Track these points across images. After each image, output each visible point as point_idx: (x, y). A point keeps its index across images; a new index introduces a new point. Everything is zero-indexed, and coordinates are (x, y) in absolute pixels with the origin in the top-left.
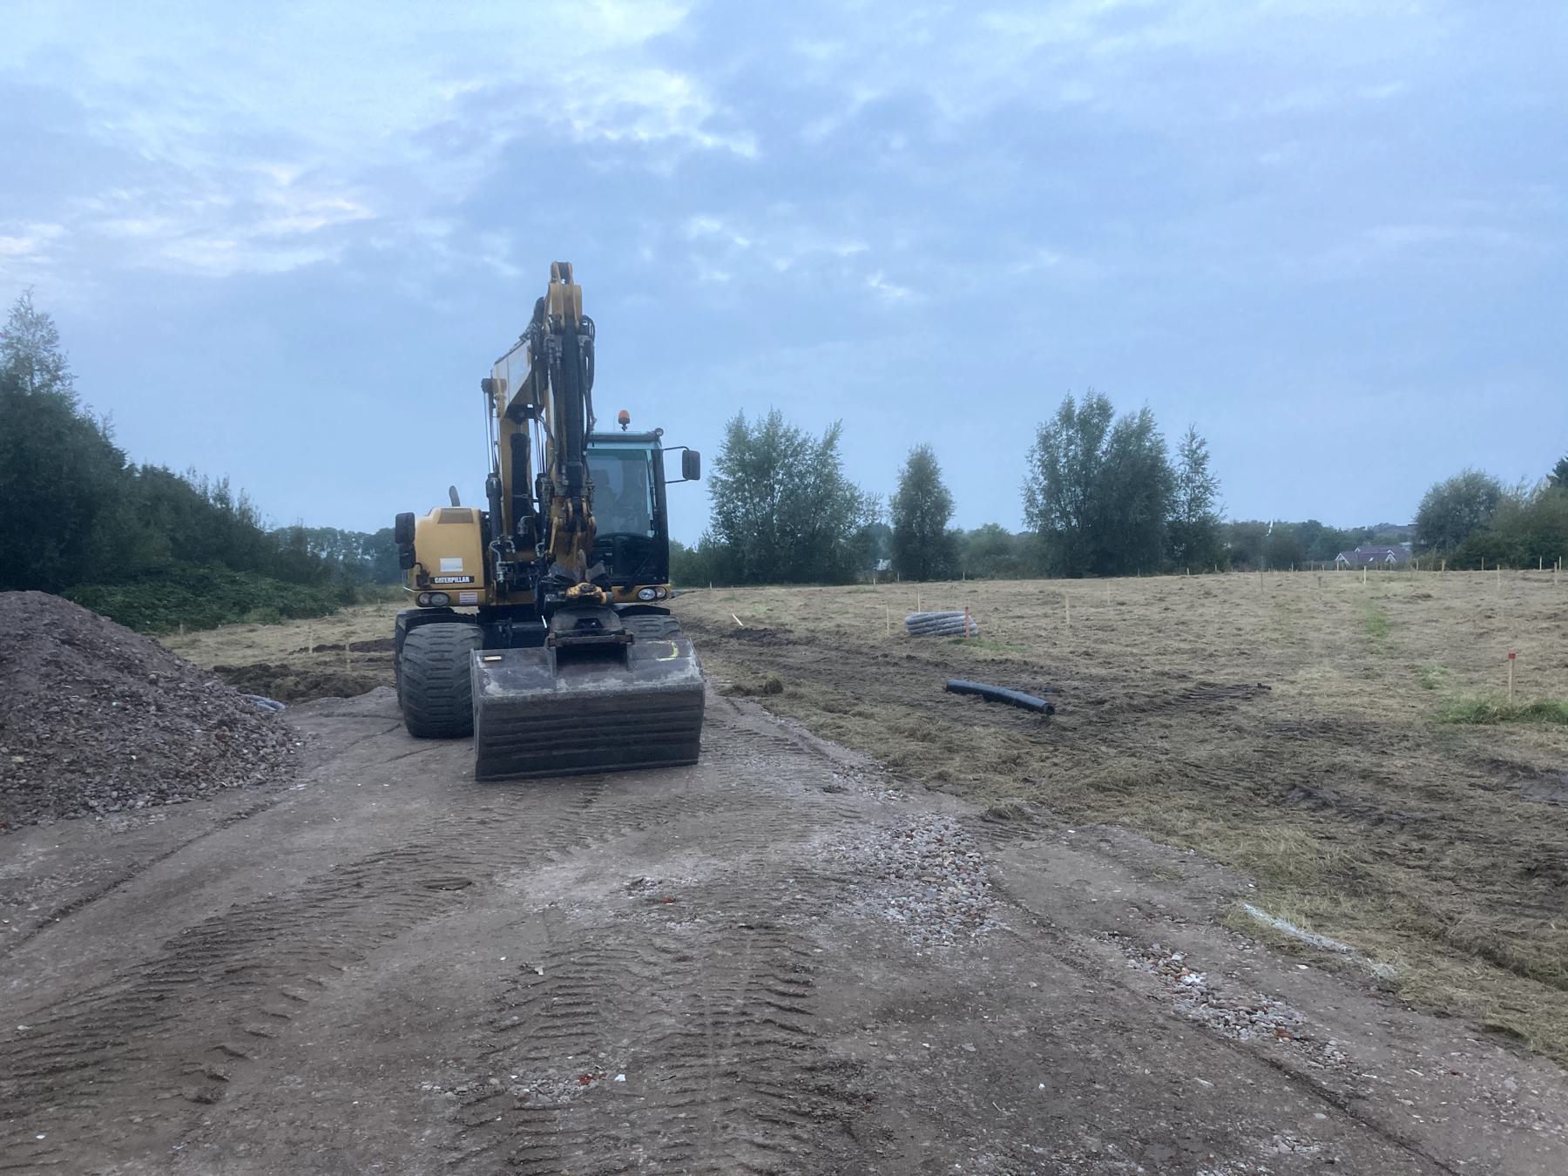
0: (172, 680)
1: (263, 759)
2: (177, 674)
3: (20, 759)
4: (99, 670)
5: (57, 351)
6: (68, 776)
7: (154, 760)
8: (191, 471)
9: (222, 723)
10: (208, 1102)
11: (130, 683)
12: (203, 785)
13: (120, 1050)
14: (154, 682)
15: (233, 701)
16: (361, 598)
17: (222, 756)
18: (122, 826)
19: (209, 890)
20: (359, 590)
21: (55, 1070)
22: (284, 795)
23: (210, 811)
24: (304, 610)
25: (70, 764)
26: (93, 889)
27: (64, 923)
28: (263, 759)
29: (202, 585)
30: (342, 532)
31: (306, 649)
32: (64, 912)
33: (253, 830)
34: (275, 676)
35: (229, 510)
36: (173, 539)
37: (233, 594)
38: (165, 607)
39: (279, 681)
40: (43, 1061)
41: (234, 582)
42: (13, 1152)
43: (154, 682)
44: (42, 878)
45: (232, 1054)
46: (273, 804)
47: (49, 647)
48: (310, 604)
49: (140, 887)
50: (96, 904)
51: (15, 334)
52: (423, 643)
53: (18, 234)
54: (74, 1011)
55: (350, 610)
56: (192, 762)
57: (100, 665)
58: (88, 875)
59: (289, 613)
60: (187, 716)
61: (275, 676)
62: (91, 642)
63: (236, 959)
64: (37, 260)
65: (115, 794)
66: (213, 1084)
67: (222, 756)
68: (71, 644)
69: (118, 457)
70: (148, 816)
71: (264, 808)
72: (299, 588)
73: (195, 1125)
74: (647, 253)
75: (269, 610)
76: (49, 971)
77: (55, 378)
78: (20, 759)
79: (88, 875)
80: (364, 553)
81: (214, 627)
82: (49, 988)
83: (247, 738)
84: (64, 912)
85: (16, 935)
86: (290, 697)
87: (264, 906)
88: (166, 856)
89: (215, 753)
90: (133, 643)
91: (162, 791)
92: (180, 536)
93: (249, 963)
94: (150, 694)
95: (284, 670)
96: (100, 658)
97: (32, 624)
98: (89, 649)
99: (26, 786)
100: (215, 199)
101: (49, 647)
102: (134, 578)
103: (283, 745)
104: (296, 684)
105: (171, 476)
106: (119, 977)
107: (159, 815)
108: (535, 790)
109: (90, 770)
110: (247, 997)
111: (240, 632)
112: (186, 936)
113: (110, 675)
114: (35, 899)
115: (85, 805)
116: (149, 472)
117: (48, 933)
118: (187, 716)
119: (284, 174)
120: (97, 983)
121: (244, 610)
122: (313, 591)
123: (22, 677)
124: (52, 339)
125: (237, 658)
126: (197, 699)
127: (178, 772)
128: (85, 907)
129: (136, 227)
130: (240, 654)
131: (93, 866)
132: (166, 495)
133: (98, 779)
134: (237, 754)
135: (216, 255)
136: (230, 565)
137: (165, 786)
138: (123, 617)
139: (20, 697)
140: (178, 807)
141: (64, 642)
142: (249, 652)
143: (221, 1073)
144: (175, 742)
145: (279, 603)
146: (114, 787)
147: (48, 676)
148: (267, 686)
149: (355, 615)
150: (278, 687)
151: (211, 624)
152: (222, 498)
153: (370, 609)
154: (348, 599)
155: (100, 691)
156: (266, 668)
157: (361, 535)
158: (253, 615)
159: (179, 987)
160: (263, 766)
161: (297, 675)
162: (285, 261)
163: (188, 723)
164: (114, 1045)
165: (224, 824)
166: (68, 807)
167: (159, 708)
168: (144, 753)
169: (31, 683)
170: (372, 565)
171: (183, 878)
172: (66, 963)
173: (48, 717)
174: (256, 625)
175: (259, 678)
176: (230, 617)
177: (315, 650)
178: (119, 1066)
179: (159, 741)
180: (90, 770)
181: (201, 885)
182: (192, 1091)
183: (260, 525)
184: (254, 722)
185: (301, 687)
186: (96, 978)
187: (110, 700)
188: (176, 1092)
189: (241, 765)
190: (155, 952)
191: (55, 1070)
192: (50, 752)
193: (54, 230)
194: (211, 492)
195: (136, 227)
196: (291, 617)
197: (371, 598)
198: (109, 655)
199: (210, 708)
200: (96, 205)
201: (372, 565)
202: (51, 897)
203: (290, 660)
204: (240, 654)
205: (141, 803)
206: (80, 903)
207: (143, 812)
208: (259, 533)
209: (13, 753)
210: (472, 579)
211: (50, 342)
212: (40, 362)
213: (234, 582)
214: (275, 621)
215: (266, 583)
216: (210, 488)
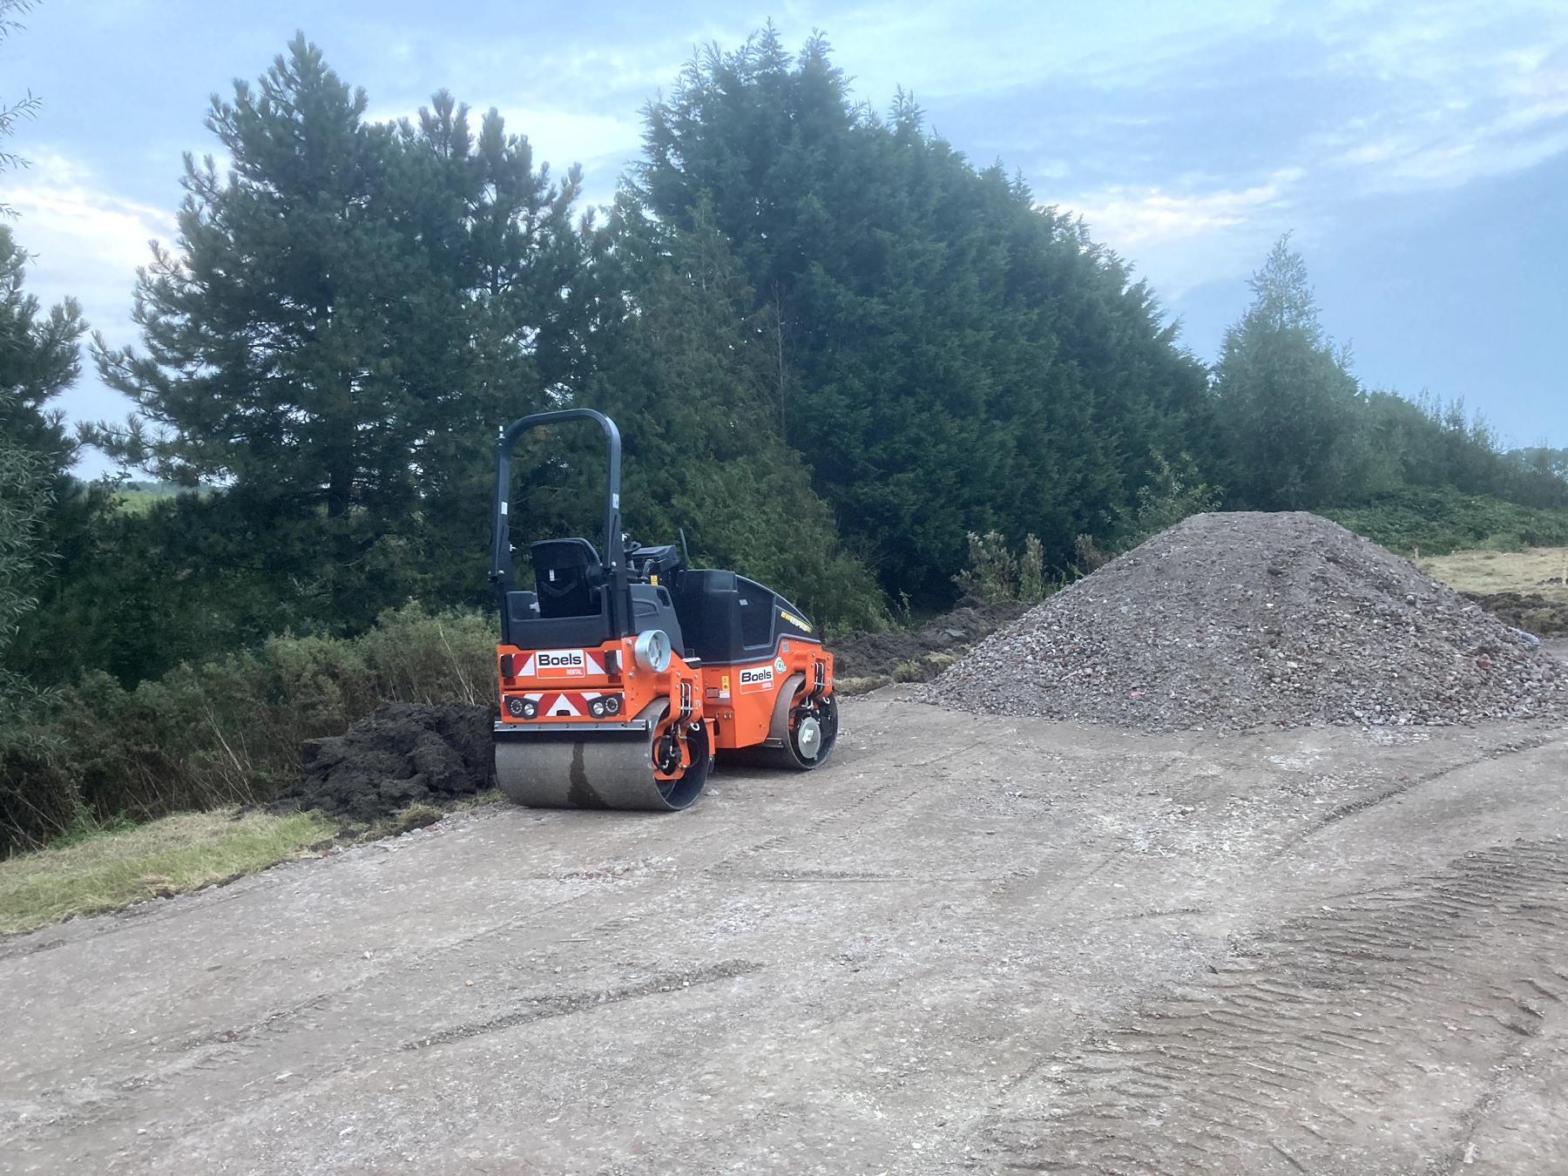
0: (1429, 602)
1: (1528, 692)
2: (1434, 597)
3: (1294, 665)
4: (1360, 588)
5: (1304, 288)
6: (1337, 685)
7: (1415, 680)
8: (1425, 393)
9: (1482, 650)
10: (1523, 1032)
11: (1388, 603)
12: (1465, 711)
13: (1423, 954)
14: (1412, 603)
15: (1493, 628)
17: (1484, 683)
18: (1388, 740)
19: (1487, 819)
21: (1362, 956)
22: (1556, 733)
23: (1478, 738)
24: (1550, 537)
25: (1337, 674)
26: (1368, 795)
27: (1348, 822)
28: (1528, 692)
29: (1436, 510)
31: (1558, 580)
32: (1346, 811)
33: (1529, 764)
34: (1525, 606)
35: (1461, 431)
36: (1405, 463)
37: (1469, 520)
38: (1397, 531)
39: (1531, 612)
40: (1351, 944)
41: (1468, 506)
42: (1333, 1019)
43: (1412, 603)
44: (1322, 776)
45: (1544, 992)
46: (1544, 740)
47: (1316, 564)
48: (1556, 531)
49: (1411, 801)
50: (1372, 809)
51: (1268, 275)
53: (1262, 184)
54: (1371, 905)
56: (1452, 687)
57: (1361, 583)
58: (1361, 781)
59: (1530, 540)
60: (1447, 639)
61: (1525, 606)
62: (1353, 562)
63: (1532, 895)
64: (1278, 205)
65: (1378, 708)
66: (1525, 1017)
67: (1484, 683)
68: (1336, 562)
69: (1350, 384)
70: (1411, 734)
71: (1536, 744)
72: (1542, 514)
73: (1512, 1052)
75: (1509, 537)
76: (1341, 861)
77: (1300, 314)
78: (1294, 665)
79: (1361, 781)
81: (1446, 553)
82: (1343, 878)
83: (1510, 668)
84: (1346, 811)
85: (1307, 823)
86: (1544, 630)
87: (1553, 847)
88: (1436, 775)
89: (1477, 680)
90: (1392, 564)
91: (1422, 711)
92: (1412, 460)
93: (1545, 903)
94: (1409, 615)
95: (1536, 601)
96: (1361, 576)
97: (1302, 541)
98: (1351, 567)
99: (1300, 690)
100: (1452, 105)
101: (1316, 564)
103: (1549, 680)
105: (1400, 400)
106: (1409, 884)
107: (1422, 735)
108: (763, 777)
109: (1355, 682)
110: (1551, 938)
111: (1476, 558)
112: (1472, 860)
113: (1372, 594)
114: (1318, 793)
115: (1351, 714)
116: (1377, 398)
117: (1334, 827)
118: (1447, 639)
119: (1529, 59)
120: (1388, 884)
121: (1480, 536)
123: (1293, 590)
124: (1301, 277)
125: (1491, 586)
126: (1455, 623)
127: (1439, 694)
128: (1364, 810)
129: (1369, 153)
130: (1481, 581)
131: (1366, 773)
132: (1397, 420)
133: (1362, 691)
134: (1499, 683)
135: (1451, 165)
136: (1461, 488)
137: (1425, 707)
138: (1381, 537)
139: (1293, 609)
140: (1441, 730)
141: (1329, 560)
142: (1489, 580)
143: (1533, 1007)
144: (1434, 664)
145: (1520, 529)
146: (1377, 701)
147: (1316, 590)
148: (1517, 616)
150: (1530, 618)
151: (1445, 549)
152: (1456, 420)
155: (1363, 609)
156: (1516, 597)
158: (1490, 541)
159: (1473, 908)
160: (1529, 700)
161: (1553, 607)
162: (1526, 157)
163: (1447, 647)
164: (1416, 947)
165: (1492, 754)
166: (1337, 714)
167: (1418, 629)
168: (1405, 672)
169: (1302, 596)
171: (1457, 802)
172: (1357, 859)
173: (1317, 629)
174: (1491, 553)
175: (1510, 607)
176: (1464, 542)
178: (1424, 969)
179: (1419, 662)
180: (1355, 682)
181: (1479, 812)
182: (1505, 1017)
183: (1494, 449)
184: (1517, 653)
185: (1557, 621)
186: (1388, 879)
187: (1371, 618)
188: (1486, 1012)
189: (1505, 695)
190: (1441, 867)
191: (1362, 956)
192: (1320, 661)
193: (1294, 173)
195: (1369, 153)
196: (1532, 544)
198: (1369, 574)
199: (1469, 633)
200: (1333, 140)
202: (1332, 795)
203: (1540, 590)
204: (1481, 581)
205: (1403, 721)
206: (1359, 806)
207: (1406, 729)
208: (1492, 458)
209: (1288, 658)
211: (1299, 280)
212: (1289, 299)
213: (1468, 506)
216: (1443, 409)
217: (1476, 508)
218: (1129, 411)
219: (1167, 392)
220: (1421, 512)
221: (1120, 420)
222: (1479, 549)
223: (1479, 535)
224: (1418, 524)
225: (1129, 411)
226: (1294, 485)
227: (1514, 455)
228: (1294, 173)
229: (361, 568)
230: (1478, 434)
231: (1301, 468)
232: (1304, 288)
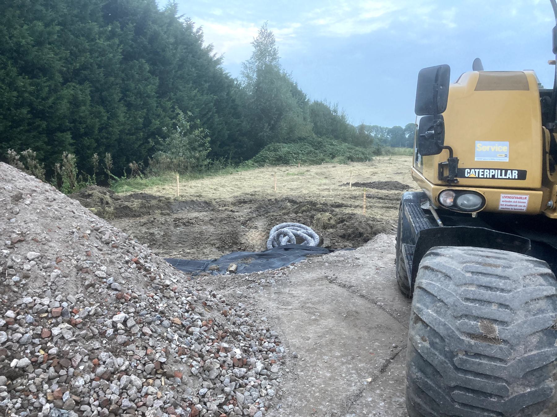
16: (383, 153)
20: (383, 149)
24: (358, 158)
29: (318, 146)
30: (380, 127)
37: (330, 150)
38: (303, 154)
41: (332, 144)
48: (361, 156)
51: (260, 41)
52: (449, 291)
55: (378, 158)
61: (318, 210)
72: (357, 148)
74: (514, 12)
80: (387, 135)
81: (320, 164)
102: (294, 141)
104: (329, 219)
116: (316, 103)
122: (363, 150)
124: (273, 42)
129: (321, 22)
145: (348, 154)
148: (312, 217)
149: (379, 161)
150: (318, 219)
152: (335, 111)
153: (386, 158)
154: (378, 153)
157: (387, 128)
158: (336, 159)
170: (389, 139)
176: (327, 160)
177: (353, 185)
185: (332, 222)
193: (297, 25)
194: (332, 108)
195: (321, 22)
196: (352, 161)
197: (388, 153)
201: (389, 139)
210: (522, 175)
213: (332, 144)
214: (345, 163)
215: (344, 145)
216: (331, 107)
217: (333, 145)
218: (181, 91)
219: (207, 85)
220: (313, 146)
221: (175, 94)
222: (332, 162)
223: (333, 156)
224: (311, 151)
225: (181, 91)
226: (266, 132)
227: (348, 125)
228: (297, 25)
229: (275, 150)
230: (342, 116)
231: (269, 125)
232: (274, 47)
